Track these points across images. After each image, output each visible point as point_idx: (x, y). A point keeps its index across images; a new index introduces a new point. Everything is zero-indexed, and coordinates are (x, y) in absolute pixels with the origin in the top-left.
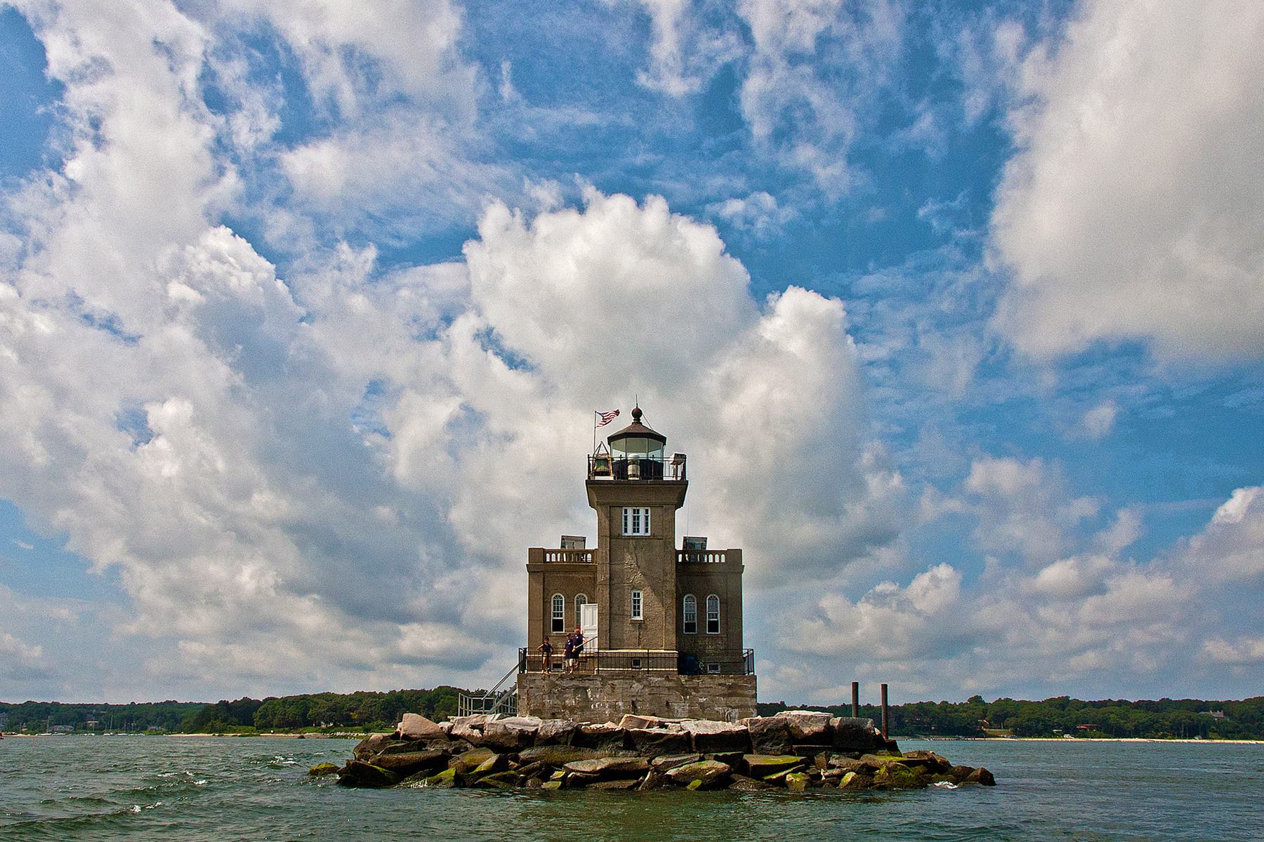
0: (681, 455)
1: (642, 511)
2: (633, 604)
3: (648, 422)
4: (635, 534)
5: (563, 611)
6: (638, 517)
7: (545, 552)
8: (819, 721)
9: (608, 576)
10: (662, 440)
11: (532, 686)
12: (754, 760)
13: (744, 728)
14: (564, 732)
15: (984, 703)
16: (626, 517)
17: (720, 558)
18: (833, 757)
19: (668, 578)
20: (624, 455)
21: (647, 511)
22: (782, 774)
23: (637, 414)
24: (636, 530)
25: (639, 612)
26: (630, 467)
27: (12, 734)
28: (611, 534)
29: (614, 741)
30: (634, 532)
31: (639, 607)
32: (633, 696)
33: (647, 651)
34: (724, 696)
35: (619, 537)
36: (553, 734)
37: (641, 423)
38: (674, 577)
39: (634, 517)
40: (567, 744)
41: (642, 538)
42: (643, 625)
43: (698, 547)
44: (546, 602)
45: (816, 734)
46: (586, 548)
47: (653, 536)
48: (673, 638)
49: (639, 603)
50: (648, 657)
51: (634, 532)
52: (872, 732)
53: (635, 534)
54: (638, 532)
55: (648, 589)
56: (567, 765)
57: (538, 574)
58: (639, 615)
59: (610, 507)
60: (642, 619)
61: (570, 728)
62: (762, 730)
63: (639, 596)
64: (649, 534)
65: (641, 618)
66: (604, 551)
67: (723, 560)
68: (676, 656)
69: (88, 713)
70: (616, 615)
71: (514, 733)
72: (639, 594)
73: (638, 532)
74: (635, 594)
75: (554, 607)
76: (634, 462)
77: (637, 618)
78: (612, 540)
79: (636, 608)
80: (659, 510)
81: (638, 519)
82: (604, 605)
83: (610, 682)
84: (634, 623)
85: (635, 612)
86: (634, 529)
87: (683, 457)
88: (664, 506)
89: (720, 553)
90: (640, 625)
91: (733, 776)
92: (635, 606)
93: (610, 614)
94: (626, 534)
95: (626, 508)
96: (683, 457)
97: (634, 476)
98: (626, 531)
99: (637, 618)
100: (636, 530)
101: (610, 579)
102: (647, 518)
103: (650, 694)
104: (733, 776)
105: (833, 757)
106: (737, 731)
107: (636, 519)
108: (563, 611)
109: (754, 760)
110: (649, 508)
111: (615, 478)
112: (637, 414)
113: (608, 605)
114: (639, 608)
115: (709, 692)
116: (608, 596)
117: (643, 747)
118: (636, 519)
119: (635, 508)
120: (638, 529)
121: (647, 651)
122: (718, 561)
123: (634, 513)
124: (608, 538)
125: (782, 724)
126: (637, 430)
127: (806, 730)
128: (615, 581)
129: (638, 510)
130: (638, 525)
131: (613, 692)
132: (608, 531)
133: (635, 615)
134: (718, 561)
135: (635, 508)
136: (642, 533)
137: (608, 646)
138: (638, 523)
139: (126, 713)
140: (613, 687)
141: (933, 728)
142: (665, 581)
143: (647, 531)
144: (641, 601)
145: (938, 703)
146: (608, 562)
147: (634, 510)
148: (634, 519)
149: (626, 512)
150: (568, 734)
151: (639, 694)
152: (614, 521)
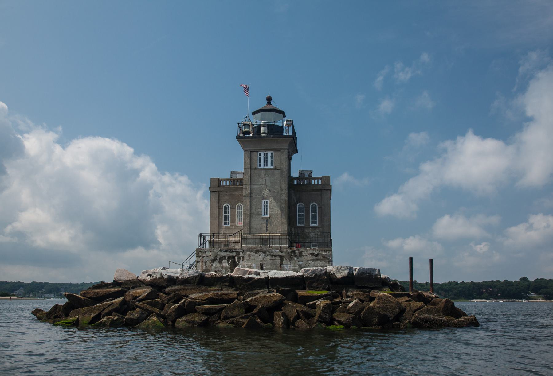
0: (290, 121)
1: (269, 154)
2: (263, 208)
3: (275, 104)
4: (266, 167)
5: (230, 214)
6: (267, 157)
7: (219, 181)
8: (345, 269)
9: (249, 192)
10: (283, 113)
11: (204, 255)
12: (300, 293)
13: (301, 274)
14: (193, 276)
15: (529, 281)
16: (260, 158)
17: (318, 182)
18: (350, 291)
19: (283, 192)
20: (258, 121)
21: (272, 154)
22: (314, 302)
23: (269, 99)
24: (266, 165)
25: (267, 212)
26: (262, 128)
27: (21, 298)
28: (251, 168)
29: (223, 282)
30: (265, 166)
31: (267, 209)
32: (261, 261)
33: (269, 235)
34: (313, 260)
35: (256, 169)
36: (187, 277)
37: (271, 104)
38: (287, 191)
39: (265, 157)
40: (194, 284)
41: (268, 169)
42: (269, 220)
43: (307, 176)
44: (220, 208)
45: (344, 278)
46: (238, 178)
47: (275, 168)
48: (285, 227)
49: (267, 207)
50: (270, 238)
51: (265, 166)
52: (379, 276)
53: (266, 167)
54: (267, 166)
55: (272, 199)
56: (190, 296)
57: (216, 192)
58: (267, 214)
59: (251, 151)
60: (268, 216)
61: (197, 274)
62: (311, 275)
63: (267, 203)
64: (273, 167)
65: (268, 216)
66: (247, 177)
67: (320, 183)
68: (288, 237)
69: (62, 288)
70: (254, 214)
71: (165, 277)
72: (267, 202)
73: (267, 166)
74: (265, 202)
75: (225, 212)
76: (264, 126)
77: (266, 216)
78: (252, 171)
79: (266, 210)
80: (278, 153)
81: (267, 159)
82: (247, 209)
83: (248, 253)
84: (263, 218)
85: (264, 212)
86: (265, 164)
87: (292, 121)
88: (281, 150)
89: (318, 178)
90: (267, 219)
91: (286, 302)
92: (264, 209)
93: (250, 214)
94: (260, 167)
95: (260, 152)
96: (292, 121)
97: (264, 133)
98: (260, 166)
99: (266, 216)
100: (266, 165)
101: (251, 193)
102: (272, 157)
103: (270, 260)
104: (286, 302)
105: (350, 291)
106: (296, 276)
107: (266, 158)
108: (230, 214)
109: (300, 293)
110: (273, 152)
111: (253, 134)
112: (269, 99)
113: (249, 208)
114: (267, 210)
115: (304, 258)
116: (249, 203)
117: (240, 286)
118: (266, 158)
119: (265, 152)
120: (267, 164)
121: (269, 235)
122: (313, 184)
123: (265, 155)
124: (250, 170)
125: (323, 272)
126: (269, 107)
127: (339, 276)
128: (253, 194)
129: (267, 153)
130: (267, 162)
131: (250, 258)
132: (250, 165)
133: (264, 214)
134: (313, 184)
135: (265, 152)
136: (269, 166)
137: (249, 232)
138: (267, 161)
139: (80, 288)
140: (250, 255)
141: (499, 295)
142: (282, 194)
143: (272, 165)
144: (268, 206)
145: (502, 281)
146: (249, 183)
147: (265, 153)
148: (265, 159)
149: (260, 155)
150: (196, 278)
151: (264, 260)
152: (253, 160)
